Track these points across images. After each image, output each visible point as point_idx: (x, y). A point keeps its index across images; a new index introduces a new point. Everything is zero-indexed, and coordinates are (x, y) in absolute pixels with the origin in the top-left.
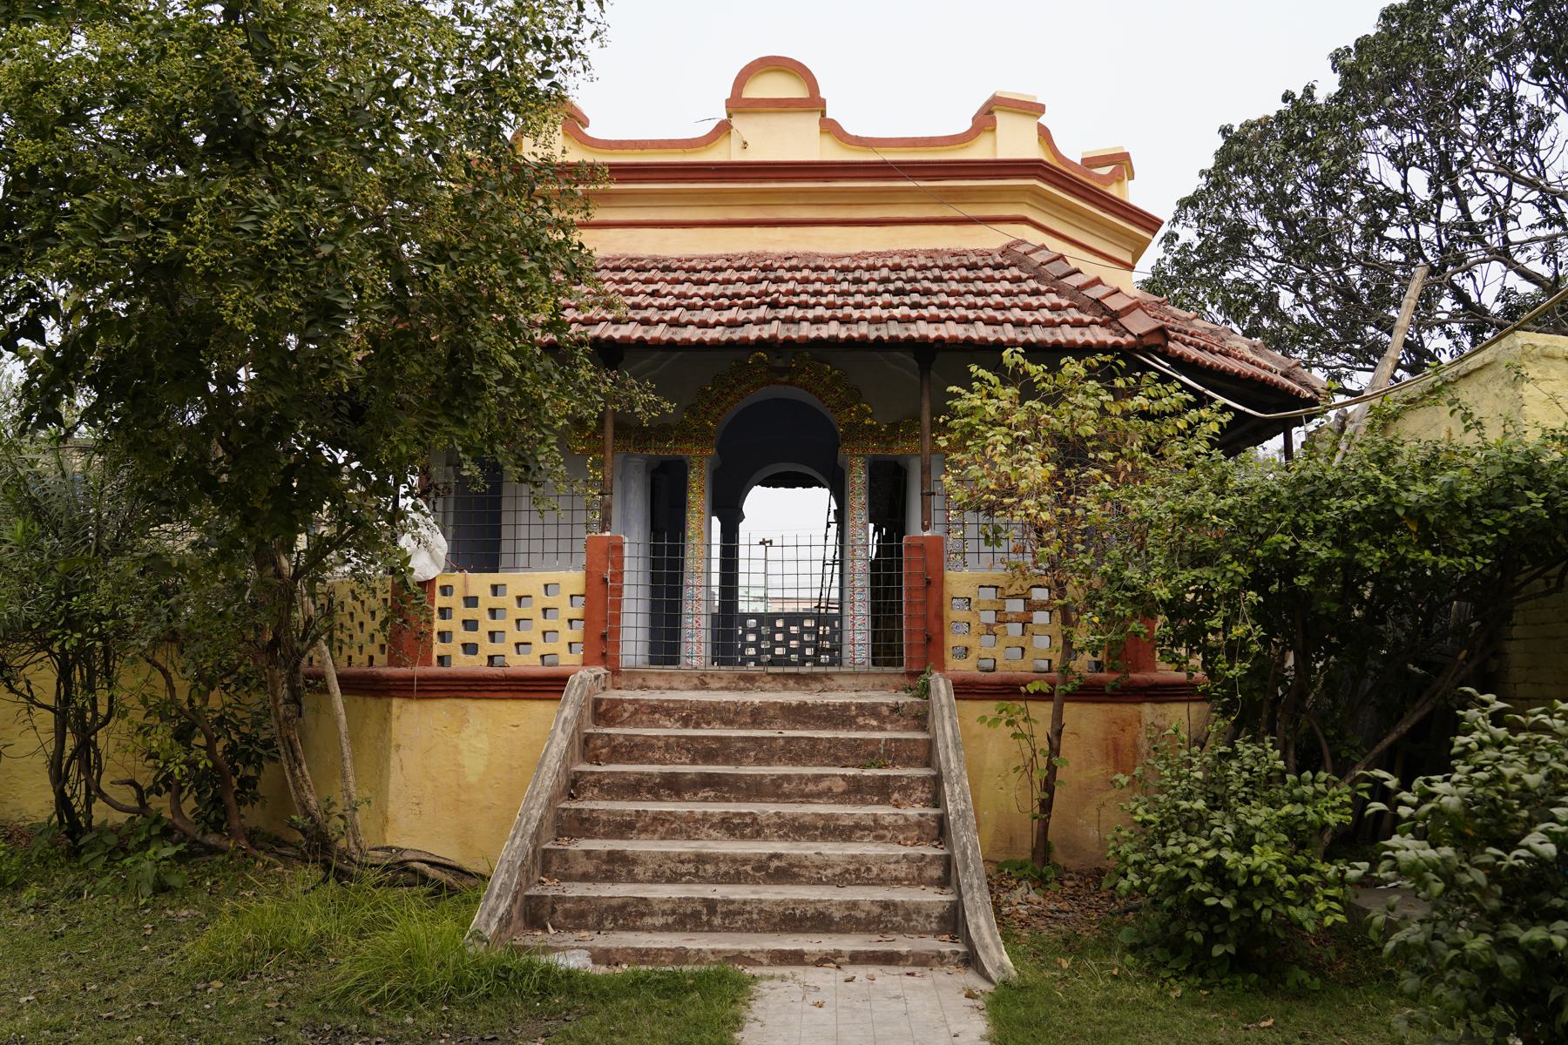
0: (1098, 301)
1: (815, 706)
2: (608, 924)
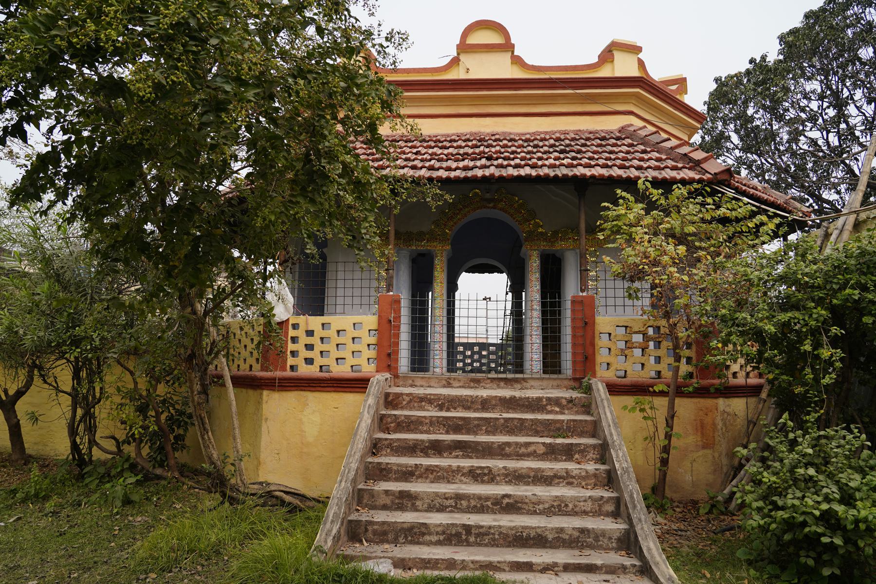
0: (685, 155)
1: (520, 398)
2: (401, 540)
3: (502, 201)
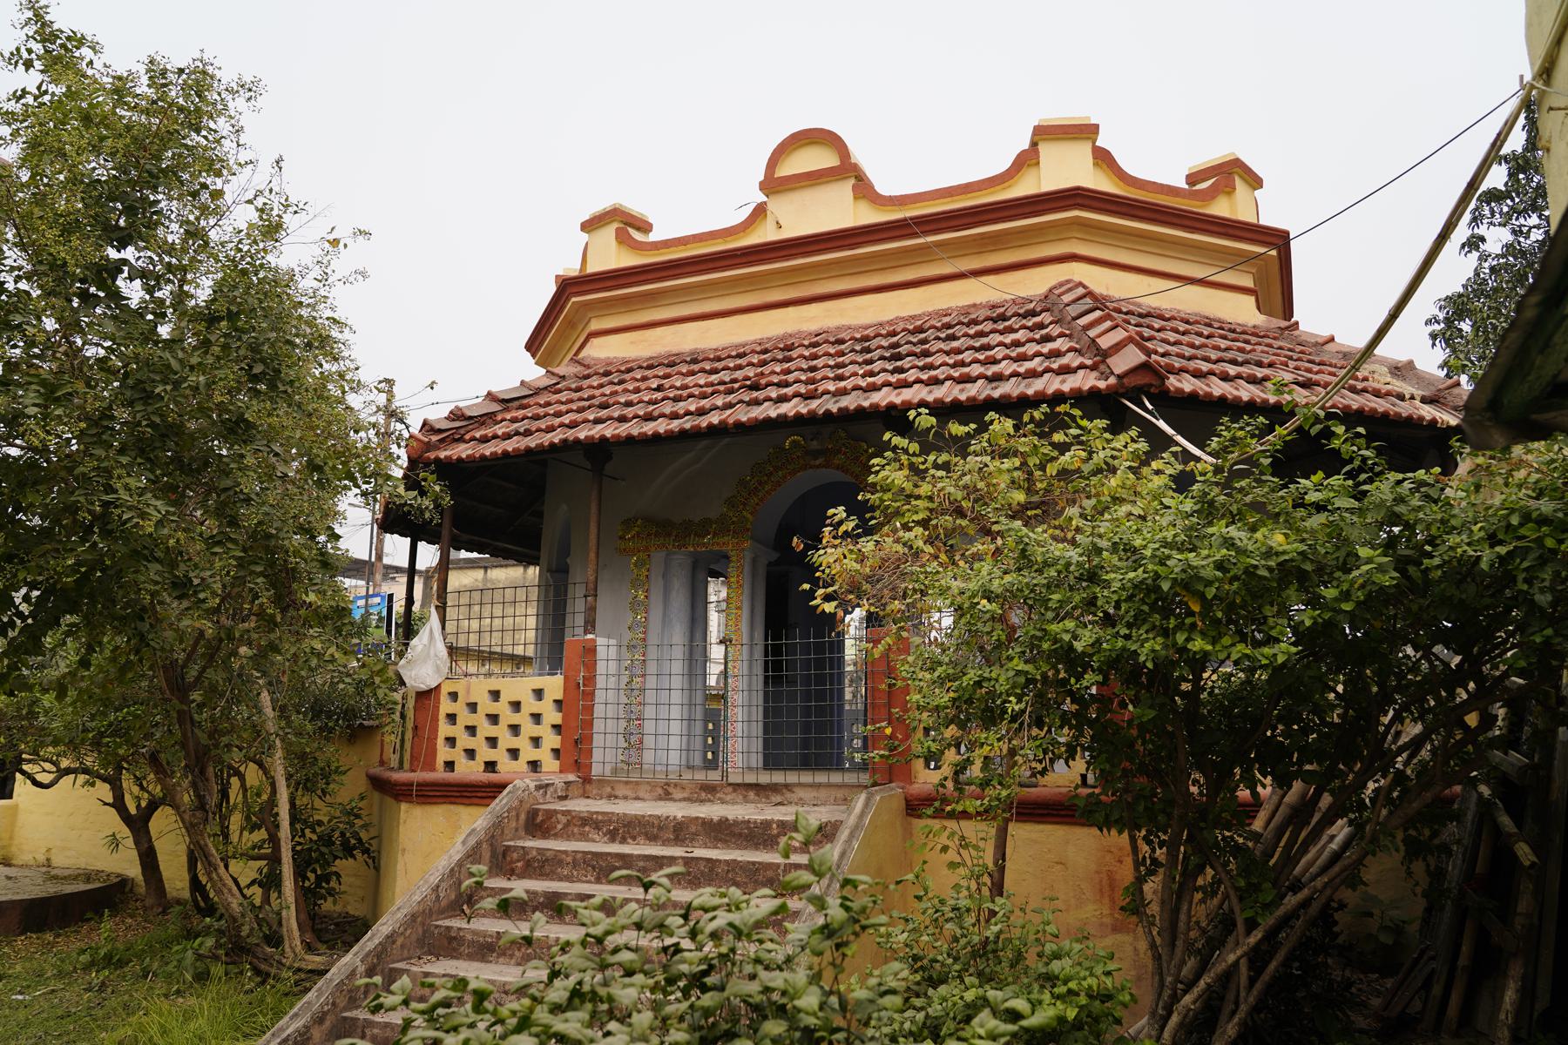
1: (736, 823)
3: (839, 451)
